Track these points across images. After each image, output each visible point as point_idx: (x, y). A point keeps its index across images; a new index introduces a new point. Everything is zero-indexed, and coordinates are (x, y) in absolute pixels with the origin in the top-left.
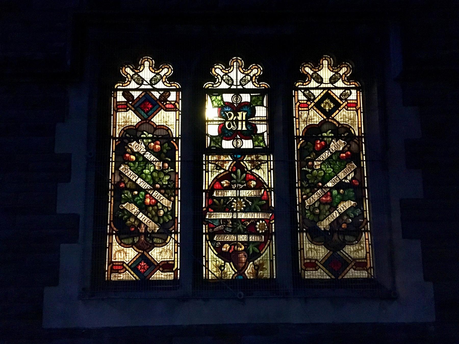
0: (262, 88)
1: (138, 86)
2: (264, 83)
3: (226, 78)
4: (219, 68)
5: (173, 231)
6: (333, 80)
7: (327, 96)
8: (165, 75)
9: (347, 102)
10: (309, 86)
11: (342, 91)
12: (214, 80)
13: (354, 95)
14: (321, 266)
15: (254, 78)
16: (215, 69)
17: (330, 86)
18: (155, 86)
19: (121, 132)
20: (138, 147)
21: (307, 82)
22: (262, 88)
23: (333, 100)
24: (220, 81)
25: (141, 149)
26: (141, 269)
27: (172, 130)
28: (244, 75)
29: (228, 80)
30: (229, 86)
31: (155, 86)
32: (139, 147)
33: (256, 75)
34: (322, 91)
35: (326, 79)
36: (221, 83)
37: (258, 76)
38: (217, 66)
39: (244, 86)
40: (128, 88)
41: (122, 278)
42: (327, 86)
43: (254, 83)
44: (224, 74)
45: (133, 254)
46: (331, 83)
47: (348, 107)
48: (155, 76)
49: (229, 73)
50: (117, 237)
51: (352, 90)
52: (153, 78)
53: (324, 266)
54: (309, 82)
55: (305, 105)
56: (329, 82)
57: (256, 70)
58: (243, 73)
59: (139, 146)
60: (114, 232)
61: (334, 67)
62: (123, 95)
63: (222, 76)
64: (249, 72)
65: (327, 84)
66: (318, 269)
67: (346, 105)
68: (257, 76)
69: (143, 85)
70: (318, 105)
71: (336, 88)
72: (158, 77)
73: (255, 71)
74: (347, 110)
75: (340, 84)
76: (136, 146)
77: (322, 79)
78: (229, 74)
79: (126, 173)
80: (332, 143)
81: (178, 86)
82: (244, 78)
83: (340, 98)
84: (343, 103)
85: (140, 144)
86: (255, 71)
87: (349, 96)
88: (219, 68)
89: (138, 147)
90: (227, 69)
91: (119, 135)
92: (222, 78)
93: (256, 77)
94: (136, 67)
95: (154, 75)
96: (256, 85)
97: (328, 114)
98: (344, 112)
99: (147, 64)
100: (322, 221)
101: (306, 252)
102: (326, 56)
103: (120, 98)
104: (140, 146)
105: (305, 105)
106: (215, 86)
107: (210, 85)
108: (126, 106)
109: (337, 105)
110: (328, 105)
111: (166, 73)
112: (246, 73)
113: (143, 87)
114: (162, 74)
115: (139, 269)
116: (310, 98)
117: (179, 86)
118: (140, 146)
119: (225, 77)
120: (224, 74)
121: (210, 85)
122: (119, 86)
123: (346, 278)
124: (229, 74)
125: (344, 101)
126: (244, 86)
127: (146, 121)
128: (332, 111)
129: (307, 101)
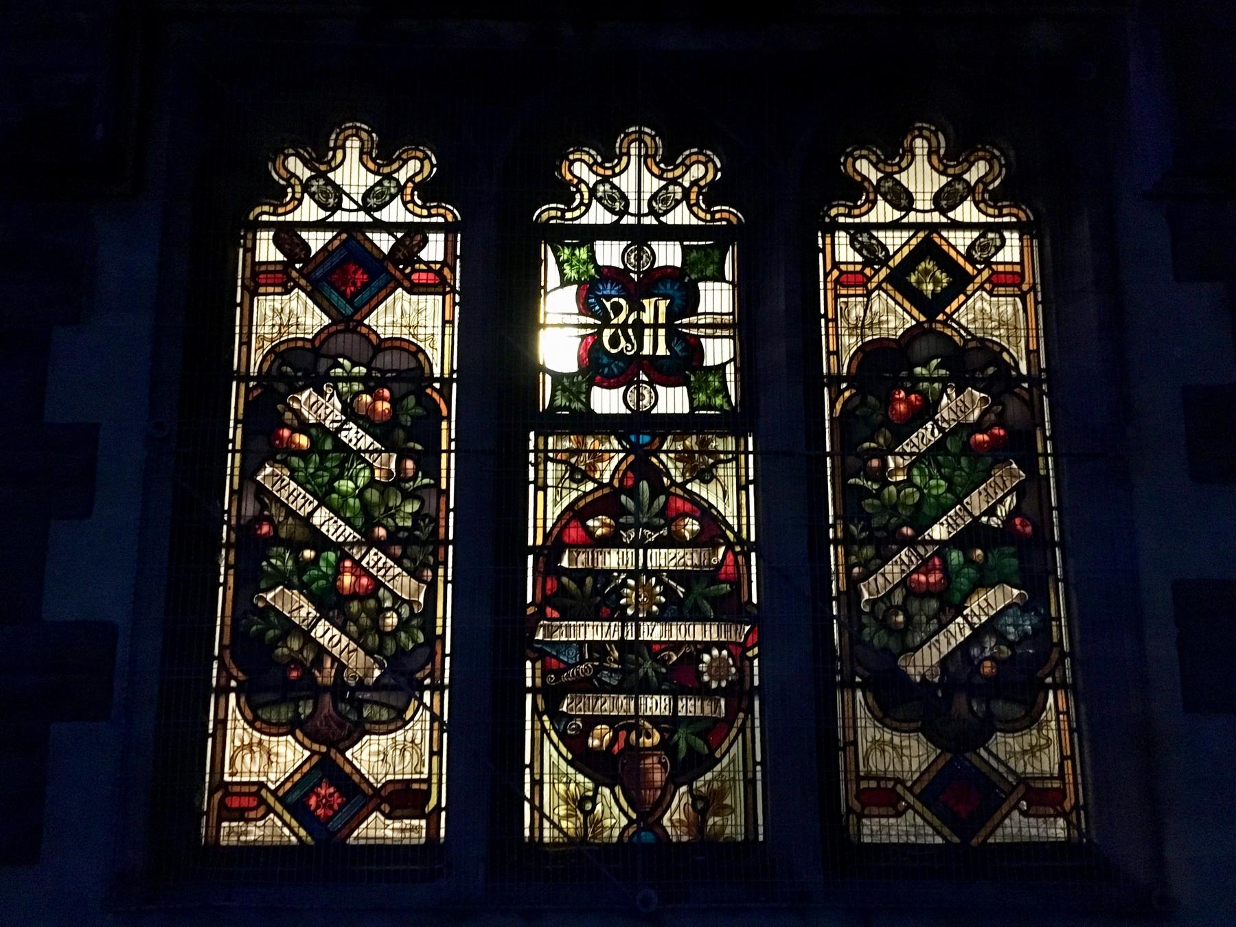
0: (719, 223)
6: (372, 200)
8: (410, 179)
12: (568, 200)
14: (279, 808)
16: (572, 163)
18: (377, 215)
22: (719, 223)
26: (318, 807)
27: (429, 352)
30: (615, 218)
31: (377, 215)
33: (702, 183)
36: (588, 206)
39: (662, 219)
42: (928, 218)
44: (599, 178)
49: (615, 175)
54: (296, 203)
63: (591, 186)
68: (704, 187)
73: (697, 171)
78: (616, 181)
82: (378, 188)
86: (697, 171)
87: (998, 249)
88: (581, 160)
90: (607, 165)
103: (267, 250)
106: (568, 215)
107: (553, 213)
108: (860, 277)
114: (402, 176)
116: (873, 255)
120: (599, 178)
121: (553, 213)
124: (616, 181)
126: (662, 219)
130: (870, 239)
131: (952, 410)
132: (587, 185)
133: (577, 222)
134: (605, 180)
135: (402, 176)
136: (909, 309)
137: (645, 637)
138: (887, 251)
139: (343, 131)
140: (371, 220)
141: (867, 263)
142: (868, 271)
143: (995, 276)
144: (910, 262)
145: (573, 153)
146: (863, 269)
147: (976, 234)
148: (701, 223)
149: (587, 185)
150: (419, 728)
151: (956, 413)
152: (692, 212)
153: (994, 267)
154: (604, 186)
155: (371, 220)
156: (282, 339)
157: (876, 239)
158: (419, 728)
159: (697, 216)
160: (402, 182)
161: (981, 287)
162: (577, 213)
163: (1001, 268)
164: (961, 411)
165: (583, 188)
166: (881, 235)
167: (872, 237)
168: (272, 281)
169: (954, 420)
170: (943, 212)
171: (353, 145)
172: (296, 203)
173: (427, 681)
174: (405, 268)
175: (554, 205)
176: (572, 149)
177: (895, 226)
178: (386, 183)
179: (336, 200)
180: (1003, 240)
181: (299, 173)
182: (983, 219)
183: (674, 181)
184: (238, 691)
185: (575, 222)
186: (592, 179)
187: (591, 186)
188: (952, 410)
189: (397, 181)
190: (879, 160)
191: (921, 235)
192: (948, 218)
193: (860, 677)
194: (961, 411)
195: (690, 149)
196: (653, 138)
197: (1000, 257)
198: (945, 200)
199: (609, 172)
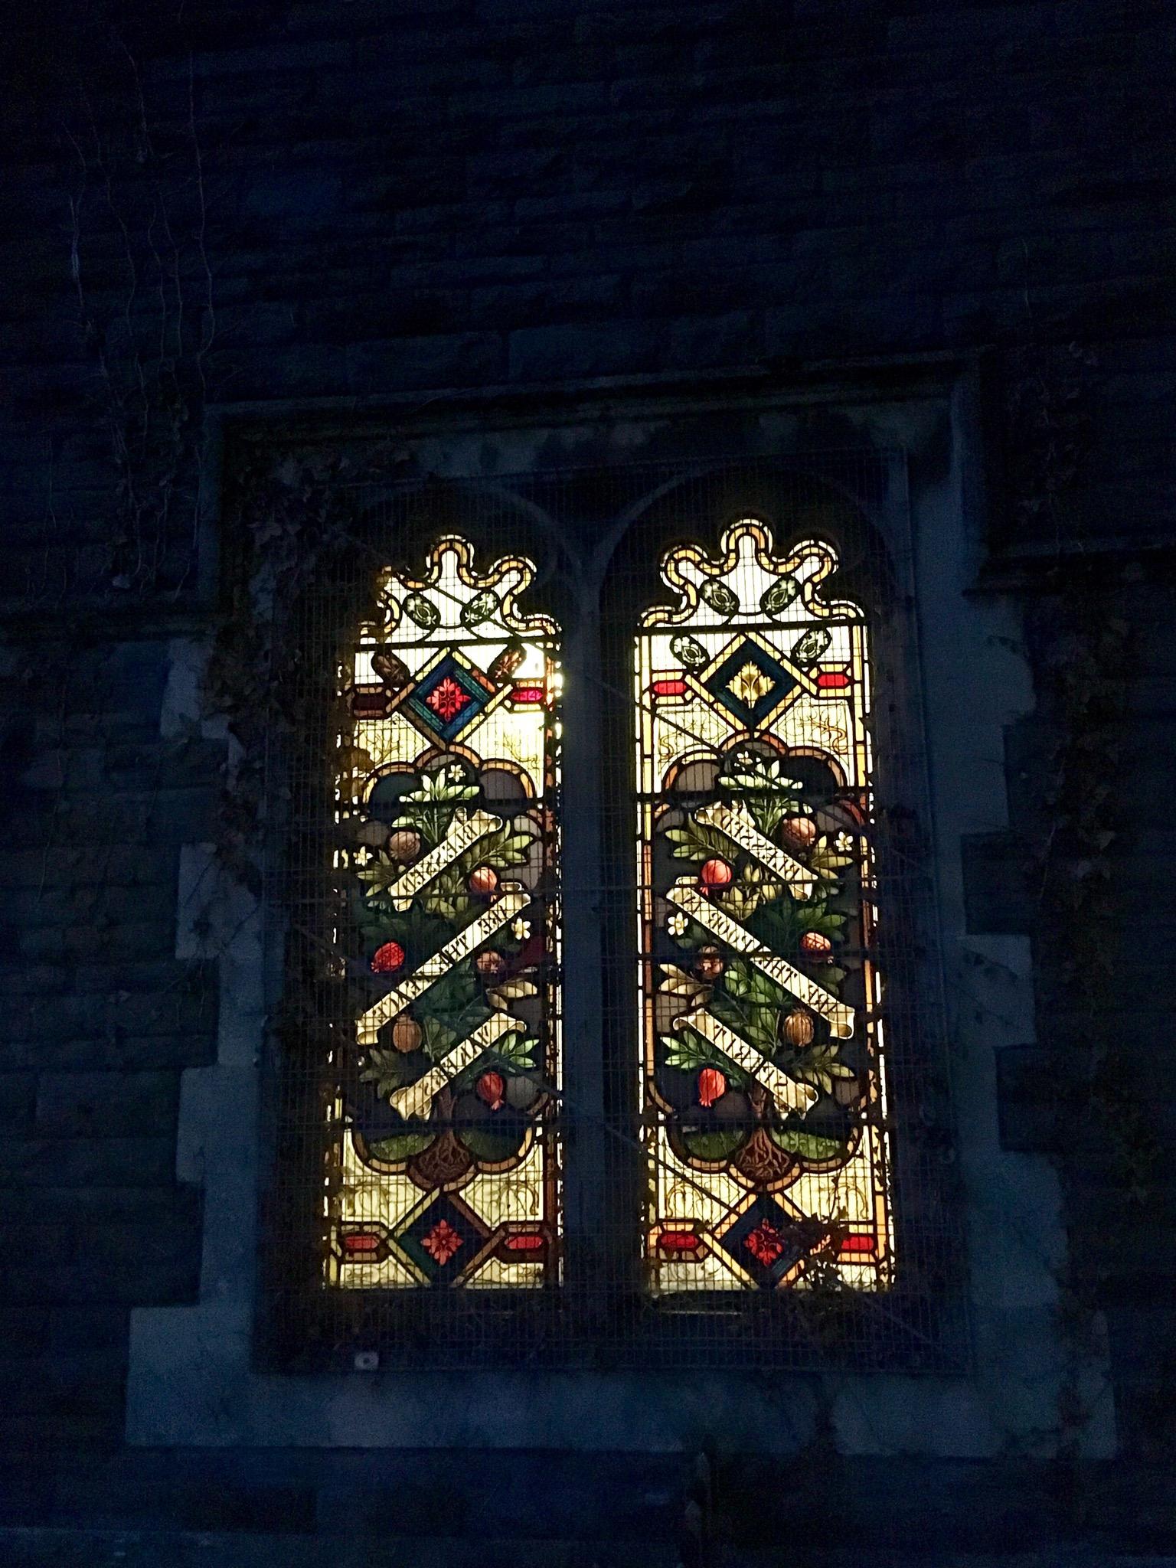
0: (837, 618)
1: (726, 618)
2: (844, 602)
3: (713, 591)
4: (688, 559)
5: (539, 1118)
6: (771, 601)
7: (448, 669)
8: (510, 592)
9: (819, 669)
10: (692, 622)
11: (797, 634)
12: (675, 600)
13: (532, 666)
14: (717, 1248)
15: (808, 588)
16: (677, 562)
17: (462, 634)
18: (776, 617)
19: (667, 774)
20: (730, 823)
21: (684, 611)
22: (837, 618)
23: (768, 666)
24: (693, 602)
25: (739, 831)
26: (760, 1249)
27: (532, 773)
28: (475, 593)
29: (779, 596)
30: (726, 618)
31: (776, 617)
32: (733, 822)
33: (816, 579)
34: (436, 650)
35: (749, 601)
36: (695, 608)
37: (821, 581)
38: (682, 554)
39: (774, 617)
40: (394, 642)
41: (375, 1280)
42: (751, 620)
43: (811, 606)
44: (410, 592)
45: (410, 1196)
46: (467, 625)
47: (514, 703)
48: (777, 585)
49: (723, 574)
50: (359, 1136)
51: (829, 629)
52: (769, 592)
53: (723, 1247)
54: (691, 610)
55: (840, 680)
56: (758, 609)
57: (682, 565)
58: (774, 572)
59: (732, 819)
60: (661, 1117)
61: (479, 568)
62: (376, 665)
63: (698, 587)
64: (790, 567)
65: (755, 614)
66: (707, 1256)
67: (507, 697)
68: (818, 584)
69: (736, 616)
70: (718, 686)
71: (481, 641)
72: (708, 590)
73: (811, 566)
74: (511, 710)
75: (795, 612)
76: (723, 819)
77: (734, 597)
78: (724, 579)
79: (506, 918)
80: (455, 824)
81: (848, 610)
82: (775, 590)
83: (794, 661)
84: (499, 690)
85: (736, 811)
86: (811, 566)
87: (824, 648)
88: (688, 559)
89: (730, 823)
90: (774, 559)
91: (664, 782)
92: (700, 593)
93: (814, 585)
94: (417, 573)
95: (775, 578)
96: (818, 612)
97: (750, 715)
98: (806, 708)
99: (747, 546)
100: (410, 1086)
101: (666, 1196)
102: (450, 537)
103: (364, 669)
104: (736, 819)
105: (840, 680)
106: (676, 618)
107: (660, 616)
108: (680, 686)
109: (784, 684)
110: (750, 683)
111: (516, 587)
112: (782, 569)
113: (439, 635)
114: (501, 590)
115: (754, 1250)
116: (393, 674)
117: (855, 610)
118: (736, 819)
119: (791, 584)
120: (410, 592)
121: (660, 616)
122: (654, 616)
123: (693, 1288)
124: (724, 579)
125: (500, 685)
126: (774, 617)
127: (752, 735)
128: (767, 703)
129: (685, 673)
130: (691, 643)
131: (460, 837)
132: (694, 586)
133: (684, 624)
134: (712, 579)
135: (501, 590)
136: (732, 722)
137: (761, 1076)
138: (708, 657)
139: (732, 531)
140: (770, 621)
141: (388, 682)
142: (389, 693)
143: (823, 677)
144: (731, 668)
145: (677, 551)
146: (684, 677)
147: (802, 632)
148: (817, 619)
149: (694, 586)
150: (859, 1170)
151: (463, 840)
152: (807, 608)
153: (822, 667)
154: (712, 585)
155: (770, 621)
156: (384, 763)
157: (697, 643)
158: (859, 1170)
159: (812, 612)
160: (501, 596)
161: (501, 703)
162: (686, 614)
163: (830, 668)
164: (468, 837)
165: (392, 602)
166: (701, 638)
167: (692, 641)
168: (531, 693)
169: (461, 847)
170: (770, 614)
171: (450, 560)
172: (691, 610)
173: (539, 1118)
174: (810, 670)
175: (661, 608)
176: (676, 548)
177: (420, 644)
178: (783, 585)
179: (435, 617)
180: (829, 637)
181: (395, 593)
182: (810, 618)
183: (787, 577)
184: (666, 1124)
185: (684, 624)
186: (698, 578)
187: (698, 587)
188: (460, 837)
189: (495, 595)
190: (703, 560)
191: (443, 653)
192: (773, 619)
193: (351, 1117)
194: (468, 837)
195: (801, 542)
196: (761, 529)
197: (828, 655)
198: (469, 615)
199: (716, 571)
